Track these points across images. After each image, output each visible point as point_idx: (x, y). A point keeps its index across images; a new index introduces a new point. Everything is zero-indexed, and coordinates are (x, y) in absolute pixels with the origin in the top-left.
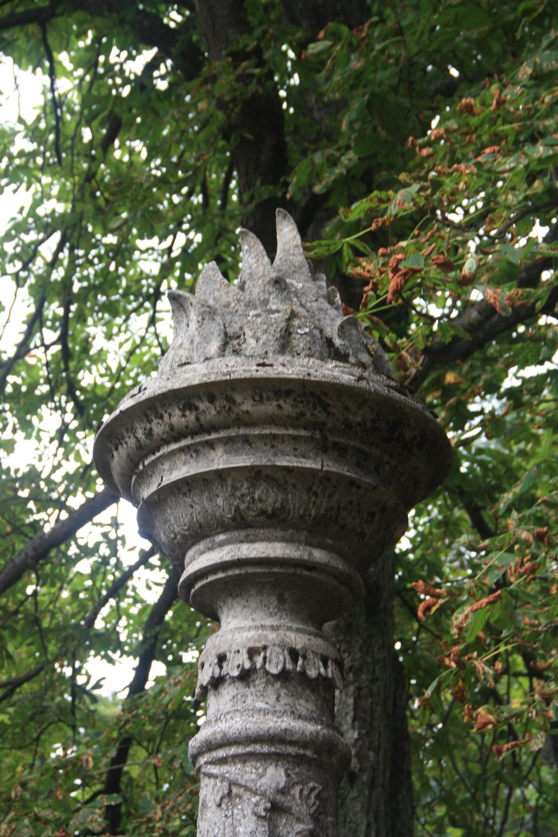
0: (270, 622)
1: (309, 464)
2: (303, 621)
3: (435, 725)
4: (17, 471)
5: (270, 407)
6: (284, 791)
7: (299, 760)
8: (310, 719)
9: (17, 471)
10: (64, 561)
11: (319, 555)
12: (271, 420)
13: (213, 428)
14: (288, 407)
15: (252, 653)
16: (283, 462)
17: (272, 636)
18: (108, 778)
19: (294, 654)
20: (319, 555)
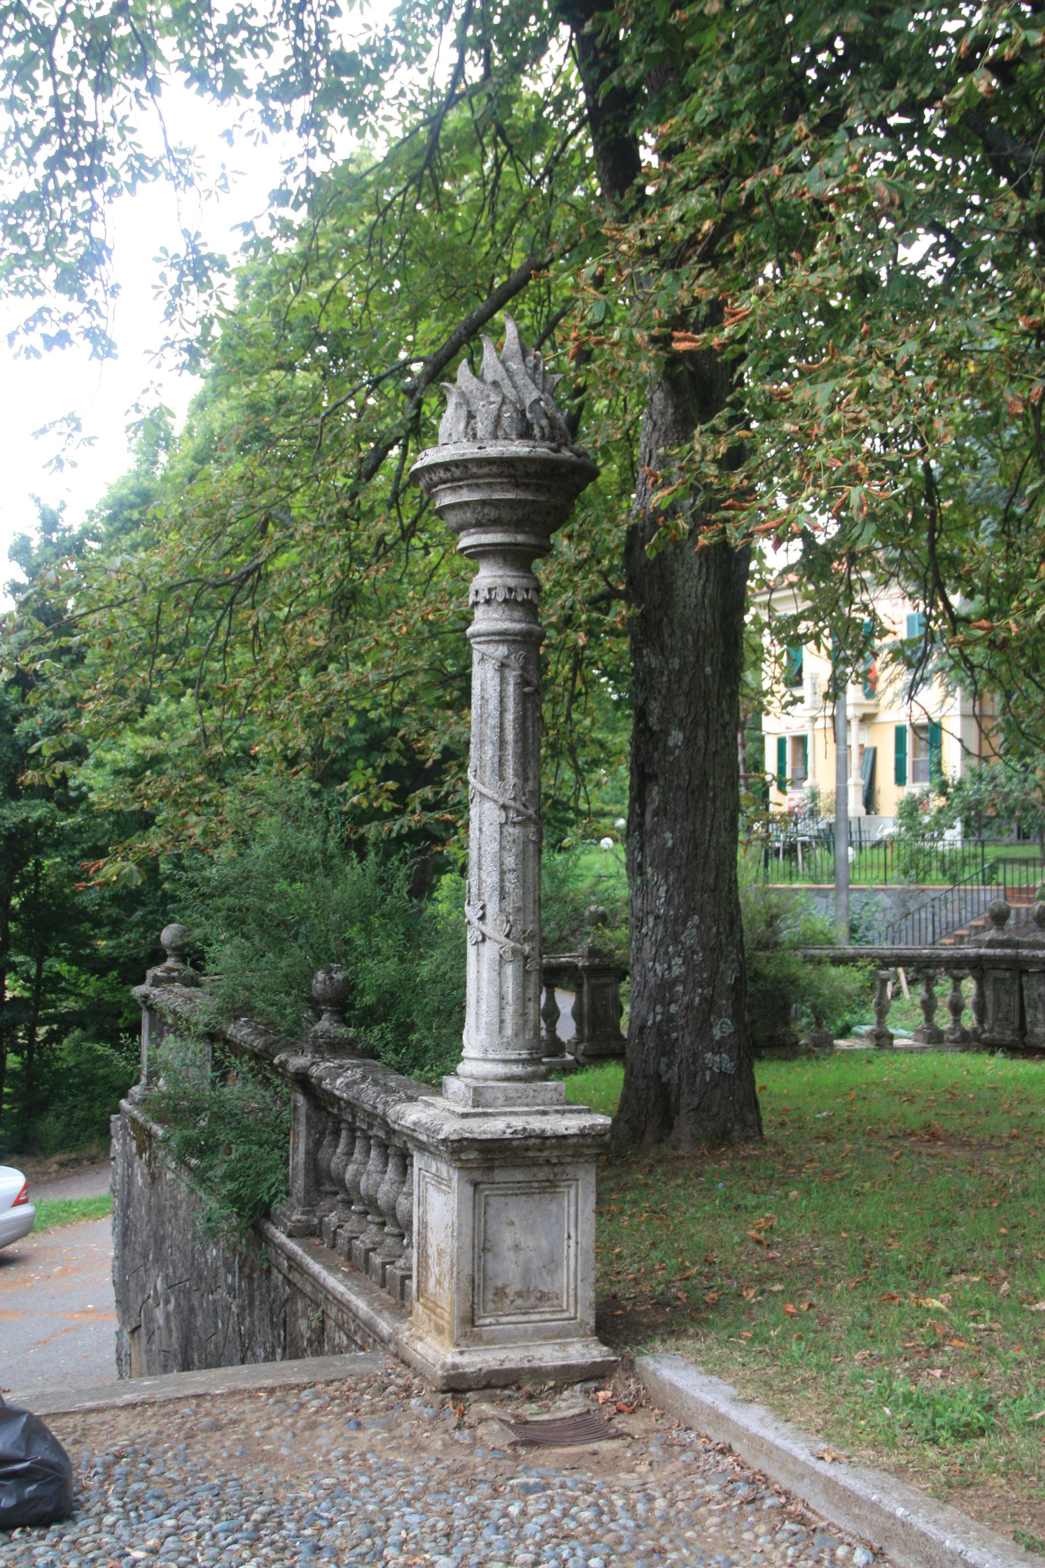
0: (500, 573)
1: (510, 496)
2: (518, 569)
3: (905, 517)
4: (205, 244)
5: (486, 470)
6: (507, 657)
7: (514, 642)
8: (520, 621)
9: (205, 244)
10: (123, 30)
11: (520, 538)
12: (488, 476)
13: (459, 480)
14: (495, 469)
15: (490, 590)
16: (496, 496)
17: (499, 581)
18: (744, 588)
19: (510, 590)
20: (520, 538)
